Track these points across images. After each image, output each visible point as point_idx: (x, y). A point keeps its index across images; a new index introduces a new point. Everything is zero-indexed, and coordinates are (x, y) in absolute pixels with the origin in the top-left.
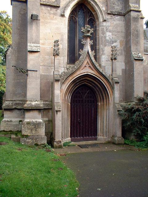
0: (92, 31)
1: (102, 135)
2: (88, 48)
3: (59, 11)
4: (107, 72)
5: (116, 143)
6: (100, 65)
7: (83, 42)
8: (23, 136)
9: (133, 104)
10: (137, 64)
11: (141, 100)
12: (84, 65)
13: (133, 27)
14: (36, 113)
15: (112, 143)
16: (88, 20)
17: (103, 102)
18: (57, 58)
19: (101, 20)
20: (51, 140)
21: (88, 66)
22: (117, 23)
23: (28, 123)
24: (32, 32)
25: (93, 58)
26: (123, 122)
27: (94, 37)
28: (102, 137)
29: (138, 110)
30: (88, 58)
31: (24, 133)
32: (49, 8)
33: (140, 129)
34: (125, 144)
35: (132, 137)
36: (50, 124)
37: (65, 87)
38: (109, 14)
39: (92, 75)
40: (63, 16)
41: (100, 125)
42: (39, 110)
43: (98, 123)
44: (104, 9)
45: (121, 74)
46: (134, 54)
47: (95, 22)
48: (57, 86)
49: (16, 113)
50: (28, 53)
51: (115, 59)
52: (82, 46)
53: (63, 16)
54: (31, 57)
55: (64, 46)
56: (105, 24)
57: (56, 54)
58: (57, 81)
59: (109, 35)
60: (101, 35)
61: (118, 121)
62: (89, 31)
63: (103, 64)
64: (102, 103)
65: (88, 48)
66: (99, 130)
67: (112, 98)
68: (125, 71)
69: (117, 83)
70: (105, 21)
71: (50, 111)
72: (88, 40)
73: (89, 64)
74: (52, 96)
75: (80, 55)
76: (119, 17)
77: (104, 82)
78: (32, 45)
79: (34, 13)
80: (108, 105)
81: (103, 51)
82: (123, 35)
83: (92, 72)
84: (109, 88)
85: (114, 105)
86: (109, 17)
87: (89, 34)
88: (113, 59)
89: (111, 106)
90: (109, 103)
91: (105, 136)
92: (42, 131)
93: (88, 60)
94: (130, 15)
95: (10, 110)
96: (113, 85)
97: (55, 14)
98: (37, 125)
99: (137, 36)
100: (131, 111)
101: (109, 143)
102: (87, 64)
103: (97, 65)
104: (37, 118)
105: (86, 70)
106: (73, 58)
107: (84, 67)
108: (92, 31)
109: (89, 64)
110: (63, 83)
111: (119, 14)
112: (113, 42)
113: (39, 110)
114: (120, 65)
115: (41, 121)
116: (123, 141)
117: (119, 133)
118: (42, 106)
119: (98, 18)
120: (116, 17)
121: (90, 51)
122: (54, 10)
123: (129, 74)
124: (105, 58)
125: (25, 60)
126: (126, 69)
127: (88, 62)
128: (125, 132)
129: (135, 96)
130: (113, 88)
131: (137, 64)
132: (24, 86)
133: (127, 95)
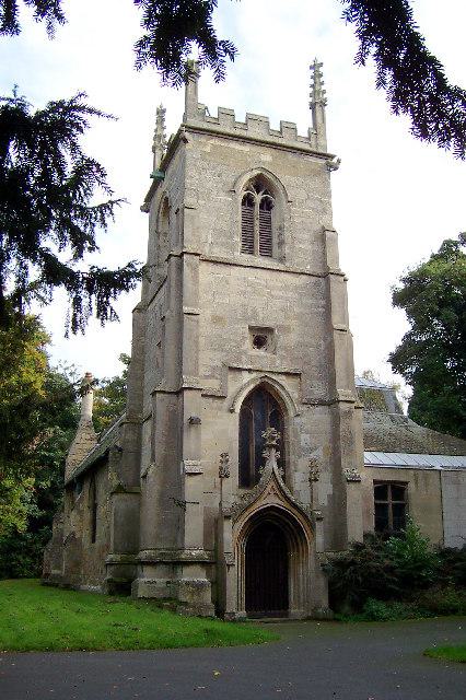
2: (272, 464)
3: (226, 404)
4: (303, 499)
5: (323, 302)
6: (291, 489)
7: (265, 454)
8: (181, 603)
9: (347, 553)
10: (351, 488)
11: (358, 547)
13: (342, 427)
14: (197, 569)
15: (315, 618)
17: (298, 551)
18: (225, 481)
19: (291, 414)
20: (220, 612)
22: (320, 416)
23: (187, 584)
24: (189, 444)
25: (280, 481)
26: (331, 585)
27: (281, 447)
29: (353, 563)
31: (183, 599)
32: (211, 400)
33: (356, 593)
34: (335, 619)
35: (347, 608)
36: (218, 586)
37: (240, 524)
40: (232, 411)
42: (203, 564)
44: (296, 395)
46: (347, 471)
48: (227, 525)
49: (161, 569)
51: (316, 480)
52: (262, 462)
53: (232, 411)
54: (190, 482)
55: (234, 459)
56: (298, 420)
57: (223, 475)
58: (228, 517)
59: (305, 439)
60: (292, 439)
61: (322, 582)
62: (273, 438)
63: (296, 487)
65: (272, 464)
68: (332, 498)
69: (319, 519)
71: (213, 567)
72: (274, 450)
74: (216, 539)
75: (260, 476)
76: (320, 408)
78: (191, 462)
79: (194, 415)
81: (295, 465)
82: (329, 436)
83: (280, 502)
85: (316, 556)
86: (305, 408)
87: (274, 443)
88: (313, 480)
89: (311, 558)
92: (208, 596)
93: (273, 483)
94: (337, 407)
95: (151, 563)
97: (220, 409)
98: (199, 587)
99: (351, 442)
100: (340, 564)
101: (308, 619)
103: (287, 491)
104: (199, 576)
105: (271, 500)
106: (248, 479)
108: (277, 436)
110: (234, 522)
111: (322, 403)
112: (312, 450)
113: (203, 564)
114: (325, 489)
116: (330, 613)
117: (325, 603)
122: (218, 402)
123: (339, 502)
124: (299, 479)
125: (180, 485)
128: (335, 599)
129: (350, 539)
130: (312, 527)
131: (351, 488)
132: (178, 526)
133: (337, 536)
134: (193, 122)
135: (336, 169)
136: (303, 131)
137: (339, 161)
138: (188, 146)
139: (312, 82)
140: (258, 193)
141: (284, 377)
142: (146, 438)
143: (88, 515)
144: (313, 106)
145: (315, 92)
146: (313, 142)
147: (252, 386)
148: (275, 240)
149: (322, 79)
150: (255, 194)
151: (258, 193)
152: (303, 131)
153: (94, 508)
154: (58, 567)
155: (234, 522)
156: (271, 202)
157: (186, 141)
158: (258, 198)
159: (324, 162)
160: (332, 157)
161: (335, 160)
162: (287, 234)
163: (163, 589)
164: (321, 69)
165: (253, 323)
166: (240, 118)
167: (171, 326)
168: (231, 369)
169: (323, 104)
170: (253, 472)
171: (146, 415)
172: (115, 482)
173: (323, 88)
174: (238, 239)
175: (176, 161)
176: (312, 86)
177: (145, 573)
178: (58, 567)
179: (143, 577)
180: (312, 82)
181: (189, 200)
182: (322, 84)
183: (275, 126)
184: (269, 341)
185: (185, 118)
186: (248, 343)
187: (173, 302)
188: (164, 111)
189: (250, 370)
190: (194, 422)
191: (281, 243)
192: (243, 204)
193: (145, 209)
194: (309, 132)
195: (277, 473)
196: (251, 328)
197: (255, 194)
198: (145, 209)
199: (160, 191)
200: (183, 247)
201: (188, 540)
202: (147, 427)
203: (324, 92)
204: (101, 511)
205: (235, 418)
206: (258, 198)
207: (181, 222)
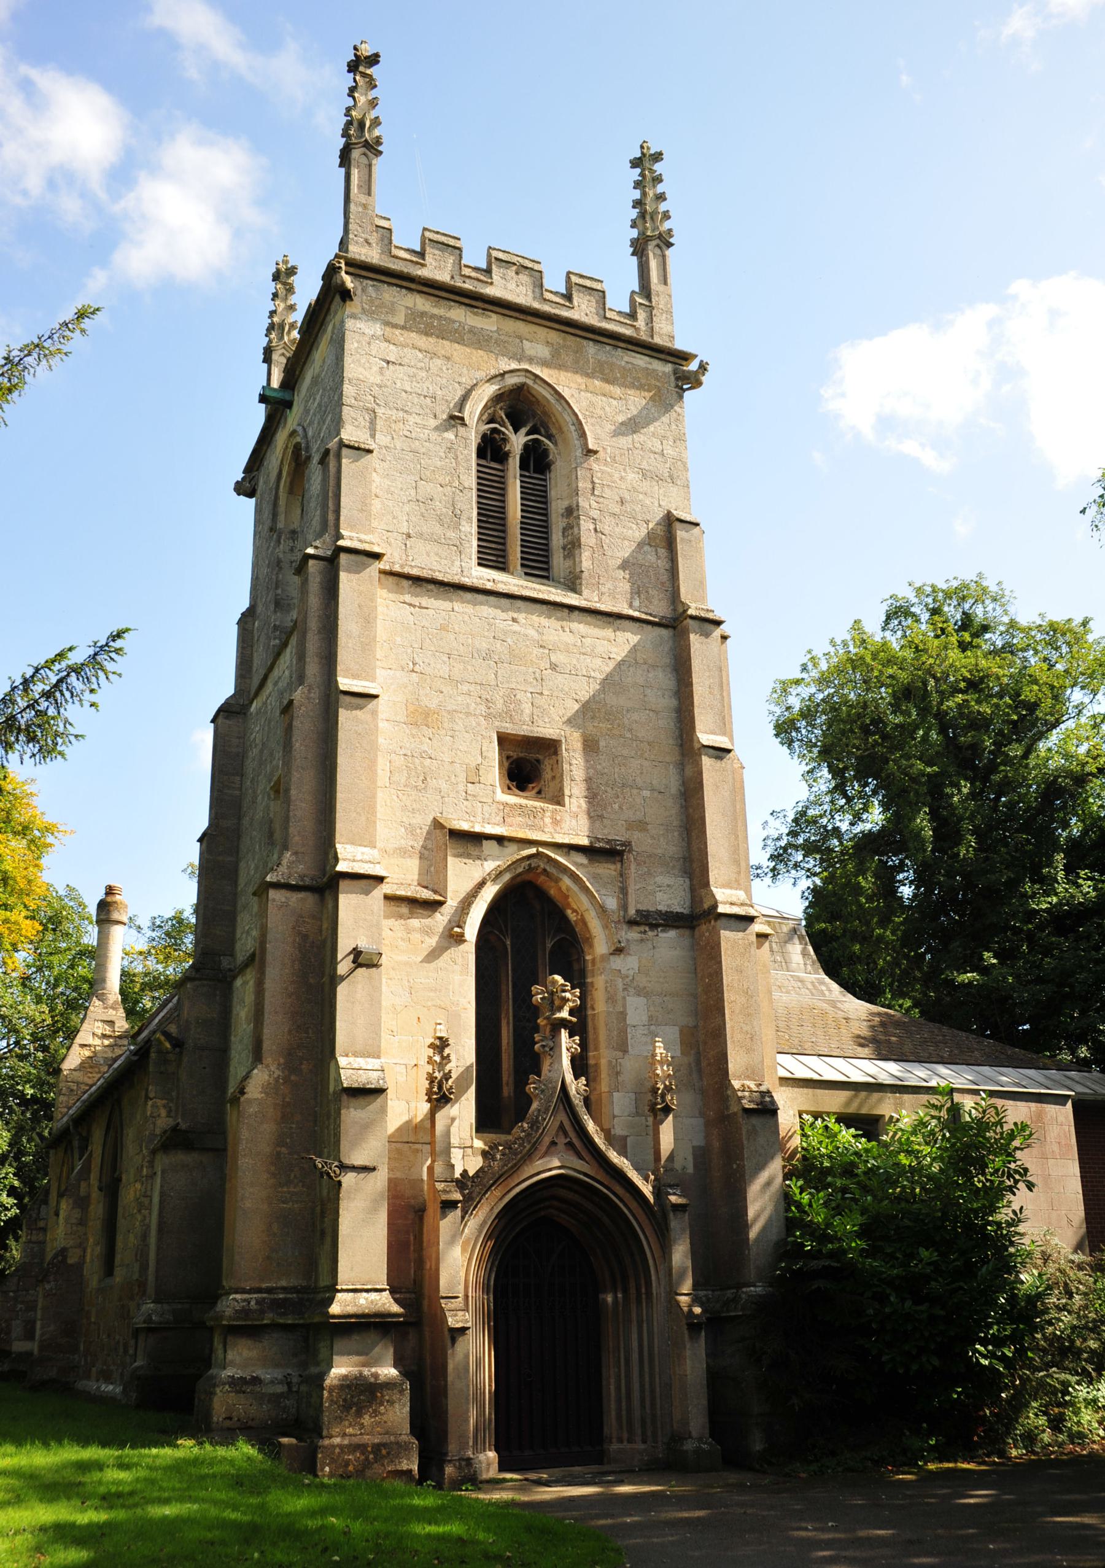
0: (572, 996)
1: (625, 1435)
3: (441, 919)
12: (547, 1140)
16: (549, 945)
21: (562, 1140)
27: (580, 1027)
28: (629, 1446)
30: (561, 1107)
38: (632, 923)
39: (581, 1177)
41: (613, 1406)
43: (604, 1383)
45: (690, 1170)
47: (581, 953)
50: (345, 1097)
56: (617, 962)
57: (440, 1097)
64: (620, 1295)
66: (613, 1406)
67: (661, 1274)
70: (619, 951)
73: (566, 1135)
77: (626, 1205)
79: (363, 944)
80: (644, 1301)
84: (649, 1231)
86: (633, 934)
90: (649, 1294)
91: (639, 1439)
93: (562, 1117)
96: (665, 1217)
102: (561, 1133)
107: (549, 1148)
108: (572, 996)
109: (566, 1135)
110: (465, 1213)
115: (393, 1372)
118: (215, 1419)
119: (589, 940)
120: (660, 935)
121: (569, 1077)
126: (638, 239)
127: (562, 1127)
134: (358, 251)
135: (697, 384)
136: (618, 301)
137: (703, 367)
138: (351, 308)
139: (637, 194)
140: (516, 431)
141: (582, 859)
142: (242, 1014)
143: (97, 1209)
144: (639, 248)
145: (643, 215)
146: (641, 323)
147: (490, 892)
148: (557, 540)
149: (660, 189)
150: (508, 431)
151: (516, 431)
152: (618, 301)
153: (112, 1189)
154: (29, 1335)
155: (465, 1213)
156: (546, 452)
157: (346, 295)
158: (517, 441)
159: (668, 368)
160: (685, 357)
161: (693, 366)
162: (586, 526)
163: (275, 1398)
164: (658, 167)
165: (509, 728)
166: (475, 257)
167: (304, 724)
168: (458, 836)
169: (665, 241)
170: (507, 1091)
171: (241, 957)
172: (163, 1122)
173: (663, 207)
174: (470, 528)
175: (322, 352)
176: (638, 204)
177: (230, 1355)
178: (29, 1335)
179: (331, 1437)
180: (637, 194)
181: (349, 433)
182: (661, 197)
183: (555, 282)
184: (547, 774)
185: (343, 244)
186: (493, 773)
187: (313, 669)
188: (292, 271)
189: (500, 840)
190: (362, 960)
191: (573, 546)
192: (481, 453)
193: (245, 488)
194: (632, 302)
195: (572, 1091)
196: (504, 740)
197: (508, 431)
198: (245, 488)
199: (281, 438)
200: (339, 536)
201: (348, 1270)
202: (244, 987)
203: (666, 216)
204: (129, 1194)
205: (467, 954)
206: (517, 441)
207: (332, 482)
